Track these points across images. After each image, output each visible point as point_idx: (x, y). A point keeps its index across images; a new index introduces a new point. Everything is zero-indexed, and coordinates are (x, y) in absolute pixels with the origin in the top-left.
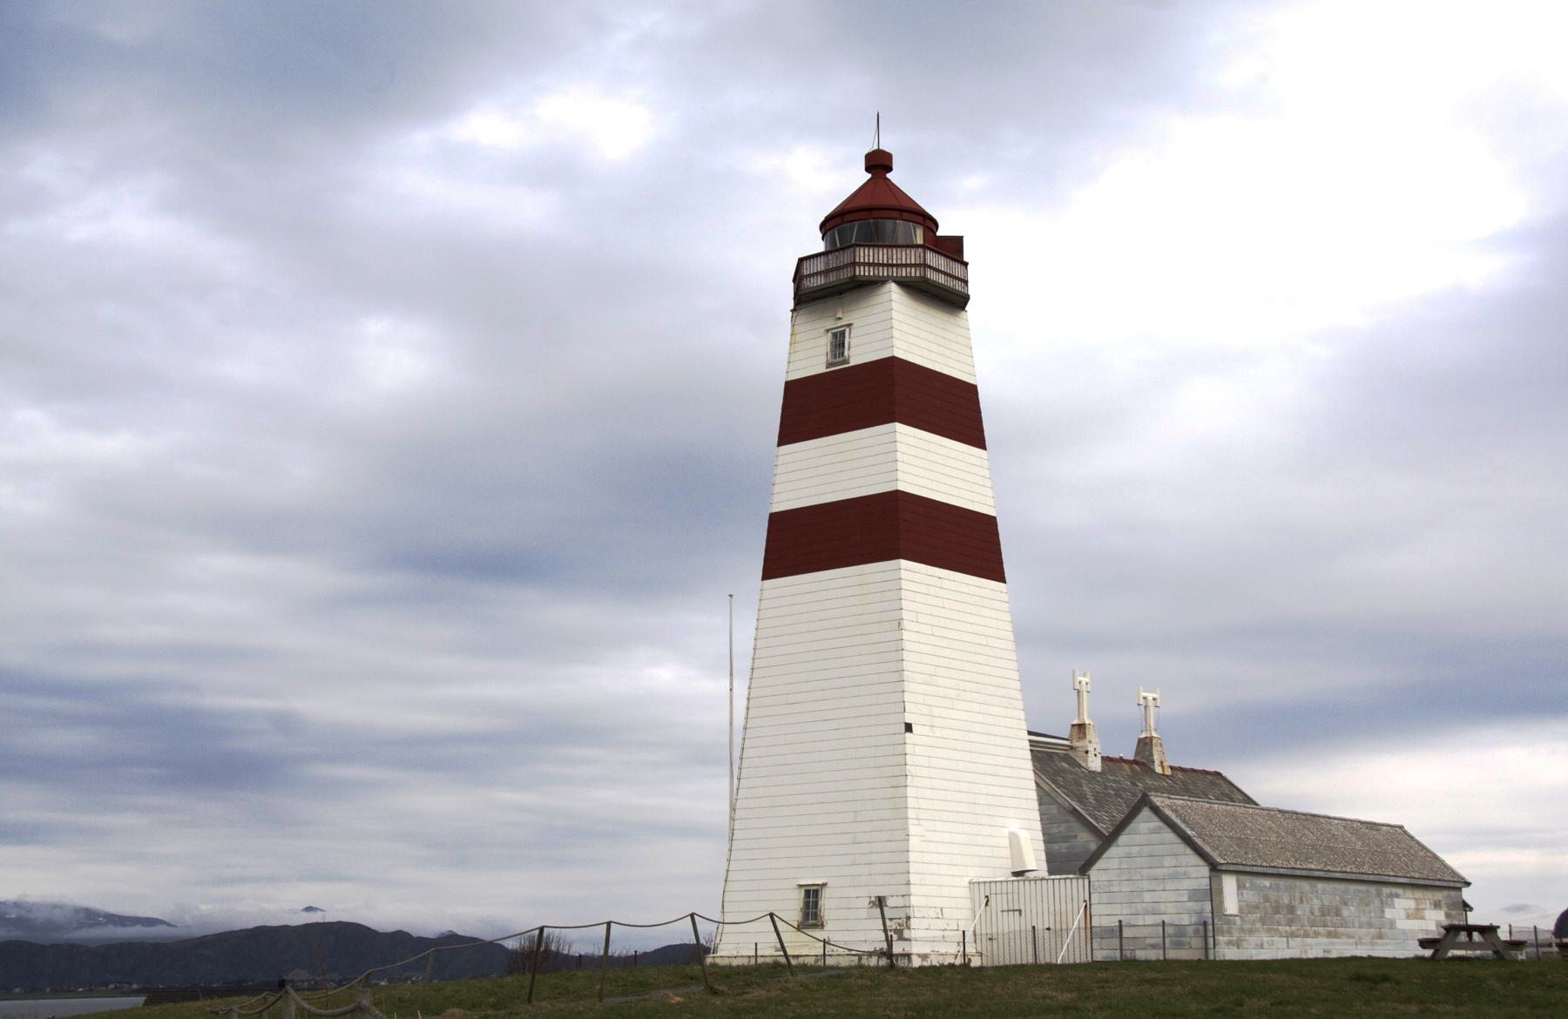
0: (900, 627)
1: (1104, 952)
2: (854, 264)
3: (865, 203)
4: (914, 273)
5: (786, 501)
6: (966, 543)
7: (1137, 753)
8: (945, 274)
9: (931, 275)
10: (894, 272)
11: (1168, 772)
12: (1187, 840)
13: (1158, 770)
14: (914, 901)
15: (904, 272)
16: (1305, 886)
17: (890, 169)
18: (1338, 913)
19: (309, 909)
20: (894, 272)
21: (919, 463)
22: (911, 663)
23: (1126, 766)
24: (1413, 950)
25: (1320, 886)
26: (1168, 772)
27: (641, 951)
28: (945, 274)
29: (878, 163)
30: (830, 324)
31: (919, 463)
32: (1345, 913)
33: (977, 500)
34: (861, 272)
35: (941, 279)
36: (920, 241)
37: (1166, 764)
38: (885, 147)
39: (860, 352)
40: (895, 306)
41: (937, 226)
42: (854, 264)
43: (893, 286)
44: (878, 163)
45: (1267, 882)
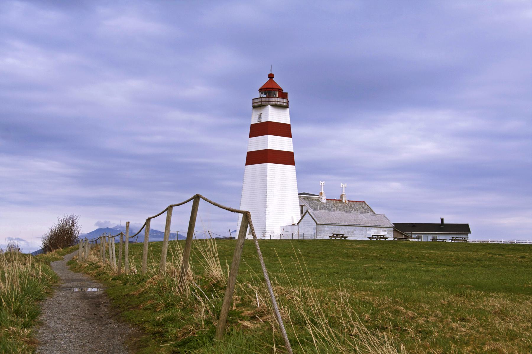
1: (301, 238)
3: (265, 87)
4: (274, 103)
5: (249, 151)
6: (285, 158)
7: (153, 231)
9: (277, 103)
10: (270, 103)
11: (347, 202)
12: (313, 219)
13: (344, 202)
14: (266, 229)
15: (272, 103)
16: (344, 227)
18: (353, 232)
19: (18, 239)
20: (270, 103)
21: (275, 143)
22: (269, 184)
24: (327, 238)
25: (348, 227)
26: (347, 202)
29: (271, 76)
31: (275, 143)
32: (355, 232)
34: (263, 103)
39: (263, 120)
43: (269, 106)
44: (271, 76)
45: (332, 226)
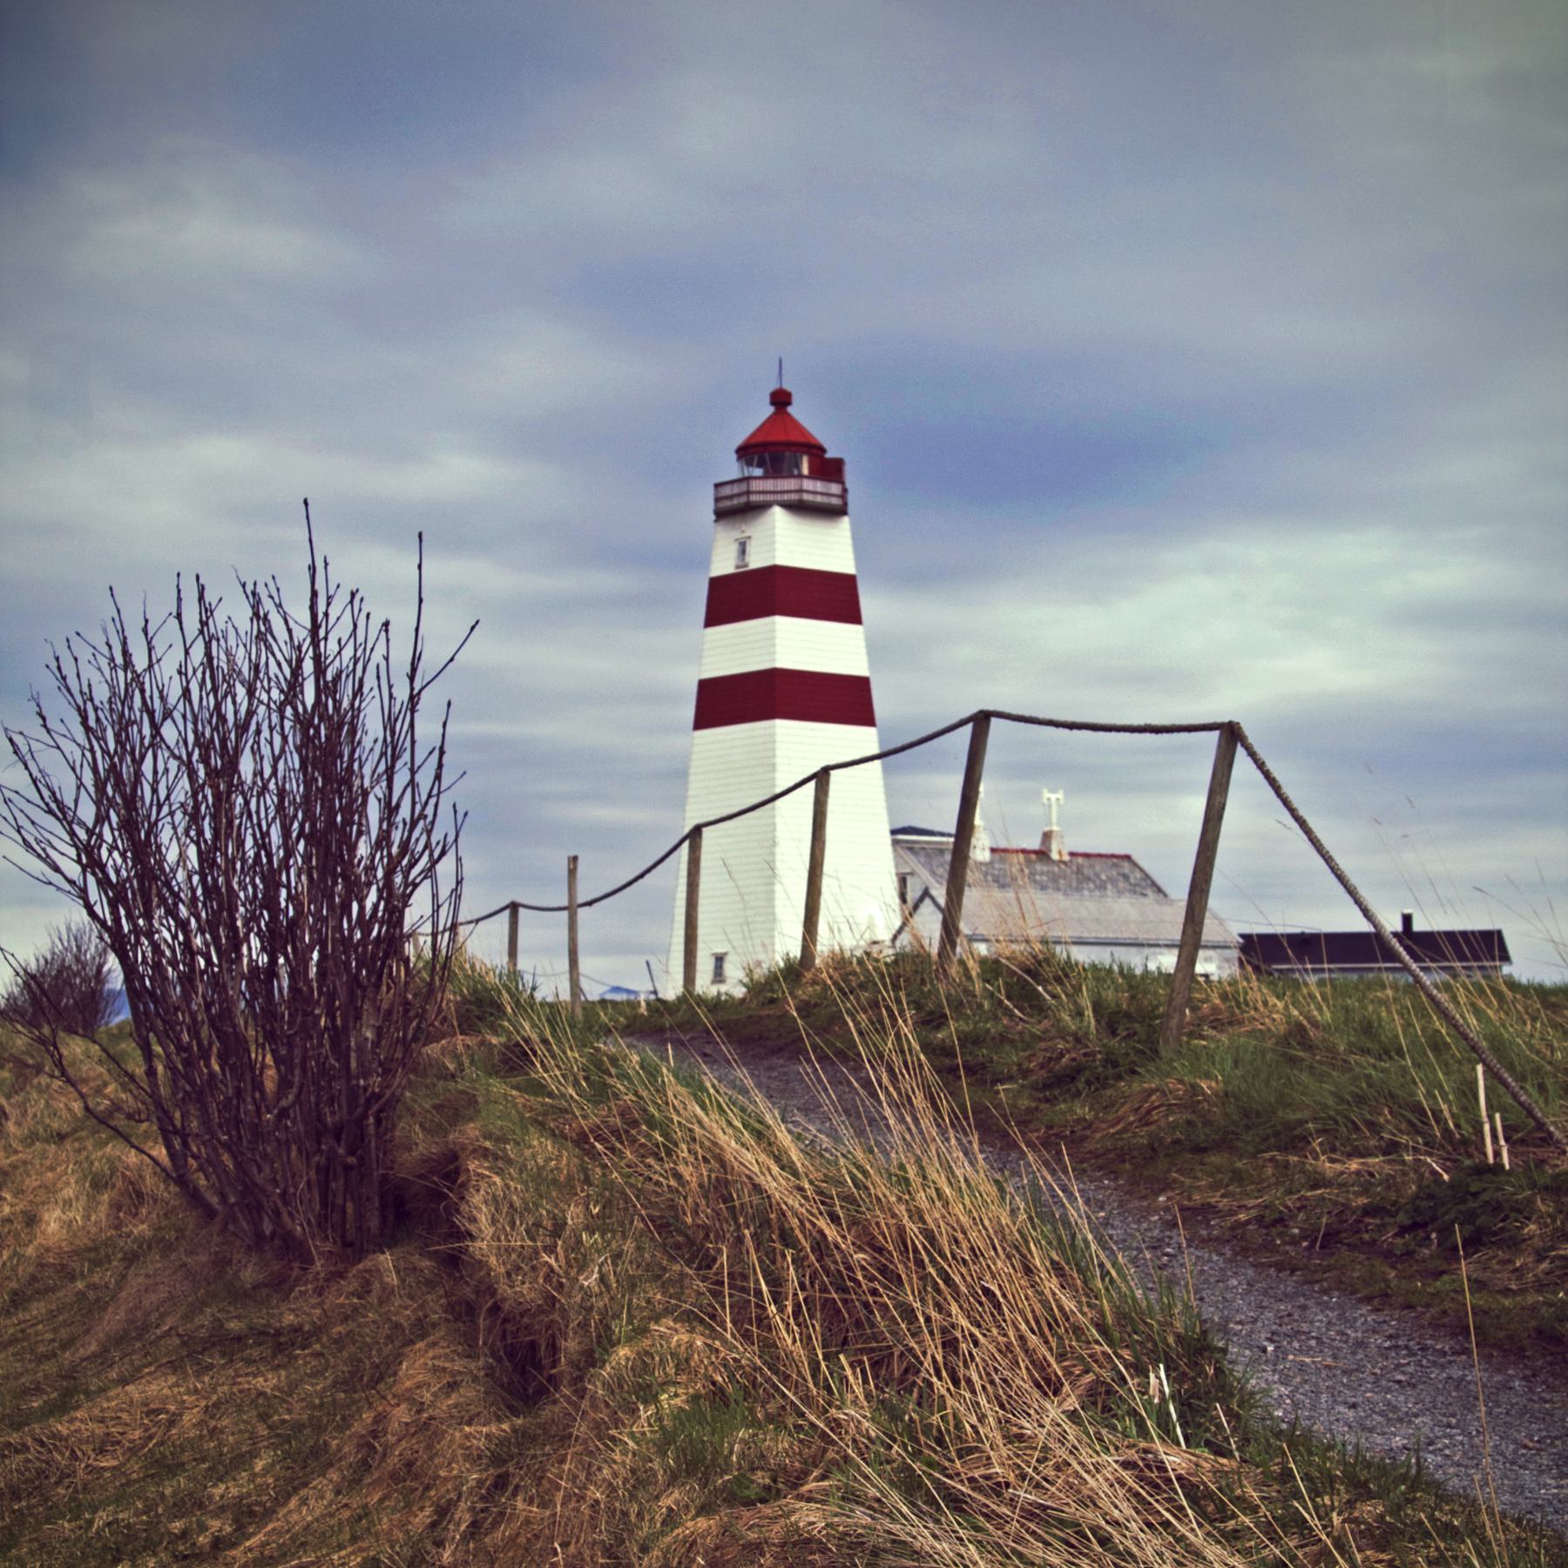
0: (774, 770)
2: (748, 493)
4: (794, 497)
8: (822, 494)
9: (806, 497)
10: (778, 497)
15: (786, 497)
17: (789, 403)
20: (778, 497)
21: (800, 644)
23: (1021, 856)
26: (1066, 858)
27: (1307, 931)
28: (822, 494)
29: (781, 399)
30: (737, 534)
33: (855, 665)
34: (754, 498)
35: (819, 499)
36: (805, 471)
37: (1065, 852)
38: (787, 387)
39: (756, 561)
40: (778, 524)
41: (823, 450)
42: (748, 493)
44: (781, 399)
